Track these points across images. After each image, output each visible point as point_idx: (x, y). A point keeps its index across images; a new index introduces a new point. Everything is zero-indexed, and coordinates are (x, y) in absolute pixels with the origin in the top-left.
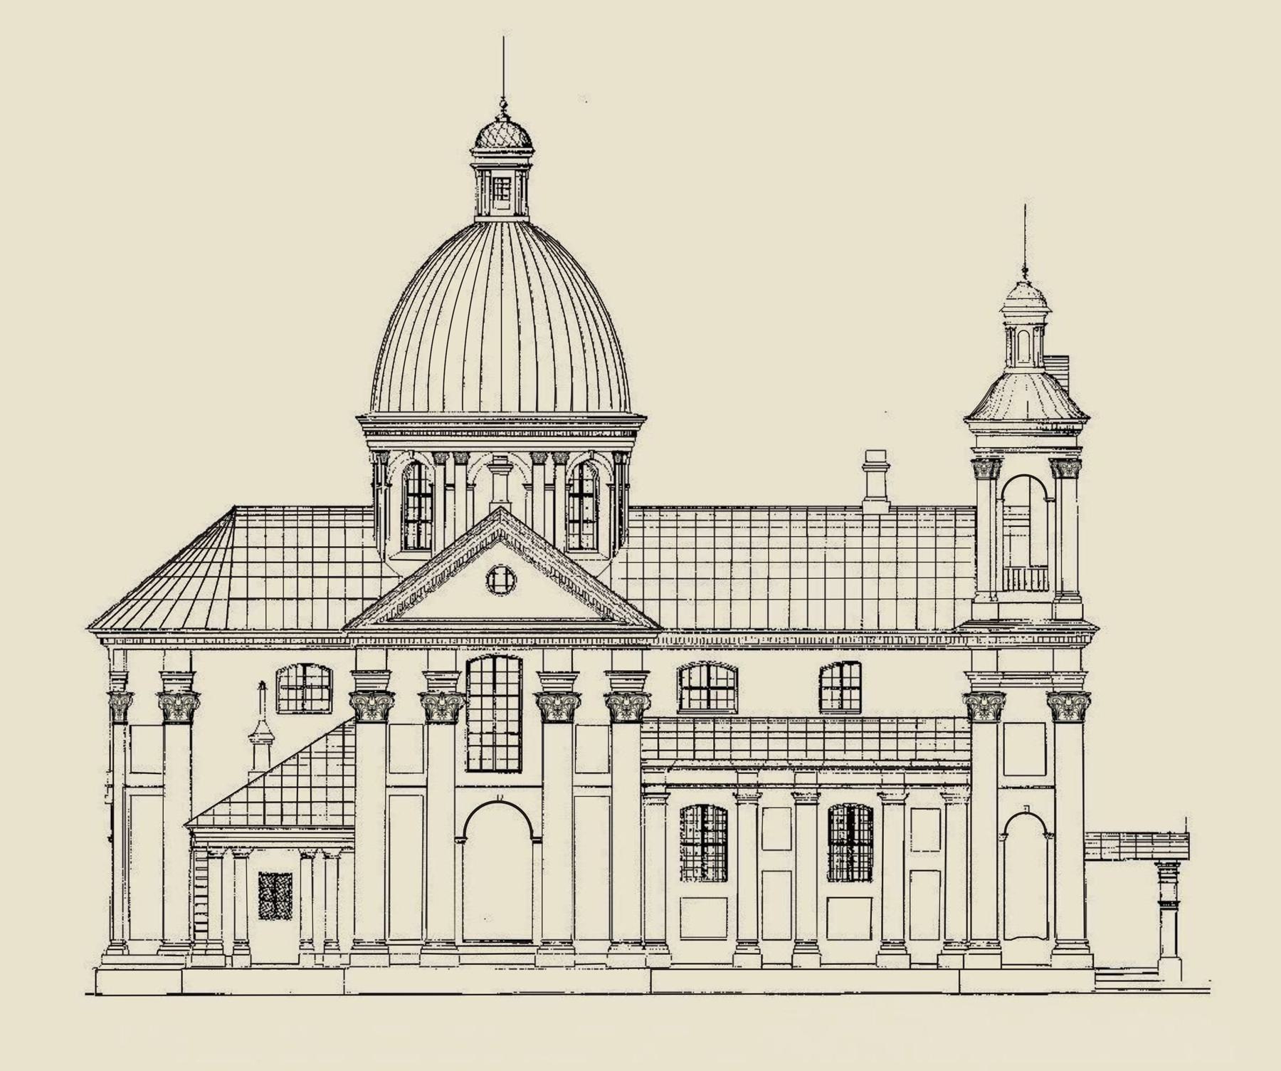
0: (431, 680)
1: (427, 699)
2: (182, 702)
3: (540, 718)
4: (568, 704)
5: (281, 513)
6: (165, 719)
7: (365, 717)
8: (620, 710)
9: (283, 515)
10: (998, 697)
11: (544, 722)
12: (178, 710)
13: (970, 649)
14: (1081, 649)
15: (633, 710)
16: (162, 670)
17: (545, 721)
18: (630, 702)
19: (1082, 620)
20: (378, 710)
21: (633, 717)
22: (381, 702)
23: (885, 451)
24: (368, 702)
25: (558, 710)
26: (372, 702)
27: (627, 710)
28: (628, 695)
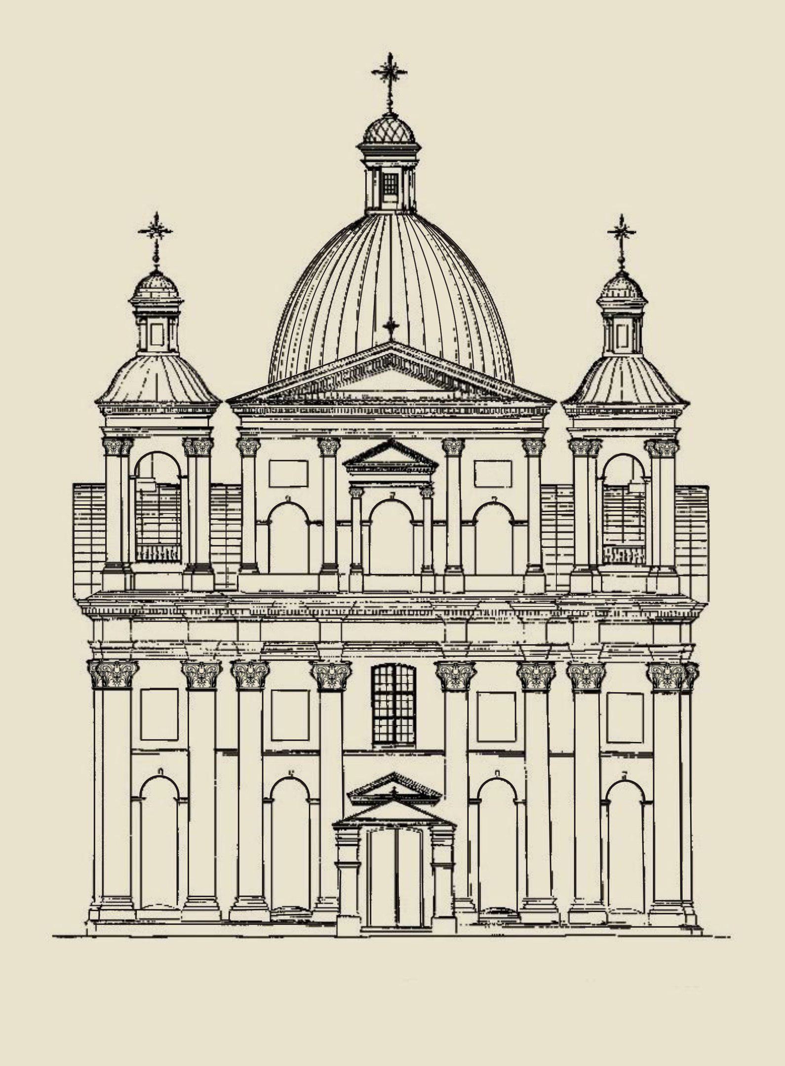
0: (95, 649)
1: (443, 668)
2: (120, 670)
3: (235, 685)
4: (595, 673)
5: (688, 524)
6: (654, 687)
7: (111, 684)
8: (662, 679)
9: (623, 526)
10: (344, 666)
11: (574, 692)
12: (456, 679)
13: (187, 621)
14: (690, 623)
15: (338, 679)
16: (91, 639)
17: (239, 689)
18: (540, 671)
19: (679, 594)
20: (542, 679)
21: (123, 684)
22: (594, 672)
23: (270, 487)
24: (533, 671)
25: (332, 679)
26: (536, 672)
27: (332, 679)
28: (457, 665)
